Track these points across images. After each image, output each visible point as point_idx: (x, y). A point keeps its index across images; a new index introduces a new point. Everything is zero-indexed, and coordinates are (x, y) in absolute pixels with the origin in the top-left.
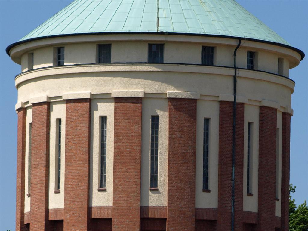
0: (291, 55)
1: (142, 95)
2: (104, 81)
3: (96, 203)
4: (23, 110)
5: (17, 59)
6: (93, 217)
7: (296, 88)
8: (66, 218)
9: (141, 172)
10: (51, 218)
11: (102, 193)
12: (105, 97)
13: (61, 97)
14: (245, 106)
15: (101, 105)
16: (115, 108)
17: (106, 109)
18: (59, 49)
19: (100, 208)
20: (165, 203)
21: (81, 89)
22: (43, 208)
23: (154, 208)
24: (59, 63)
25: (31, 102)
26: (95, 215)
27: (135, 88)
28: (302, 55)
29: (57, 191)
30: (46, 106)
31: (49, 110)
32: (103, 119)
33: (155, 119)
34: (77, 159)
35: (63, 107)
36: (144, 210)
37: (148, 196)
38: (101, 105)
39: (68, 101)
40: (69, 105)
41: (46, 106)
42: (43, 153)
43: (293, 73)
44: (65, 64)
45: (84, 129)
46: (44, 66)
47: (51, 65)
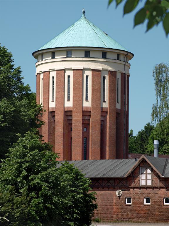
0: (128, 55)
1: (101, 69)
2: (88, 63)
3: (66, 105)
4: (39, 74)
5: (36, 57)
6: (84, 110)
7: (131, 67)
8: (74, 110)
9: (100, 95)
10: (50, 110)
11: (87, 102)
12: (70, 69)
13: (71, 68)
14: (117, 73)
15: (86, 72)
16: (92, 73)
17: (89, 73)
18: (53, 53)
19: (87, 107)
20: (90, 106)
21: (80, 66)
22: (48, 107)
23: (104, 108)
24: (53, 57)
25: (43, 71)
26: (85, 109)
27: (99, 67)
28: (133, 55)
29: (53, 101)
30: (64, 71)
31: (65, 72)
32: (69, 77)
33: (104, 77)
34: (78, 90)
35: (55, 72)
36: (102, 108)
37: (103, 103)
38: (86, 72)
39: (74, 70)
40: (74, 71)
41: (64, 71)
42: (62, 87)
43: (130, 62)
44: (56, 57)
45: (81, 79)
46: (48, 59)
47: (66, 57)
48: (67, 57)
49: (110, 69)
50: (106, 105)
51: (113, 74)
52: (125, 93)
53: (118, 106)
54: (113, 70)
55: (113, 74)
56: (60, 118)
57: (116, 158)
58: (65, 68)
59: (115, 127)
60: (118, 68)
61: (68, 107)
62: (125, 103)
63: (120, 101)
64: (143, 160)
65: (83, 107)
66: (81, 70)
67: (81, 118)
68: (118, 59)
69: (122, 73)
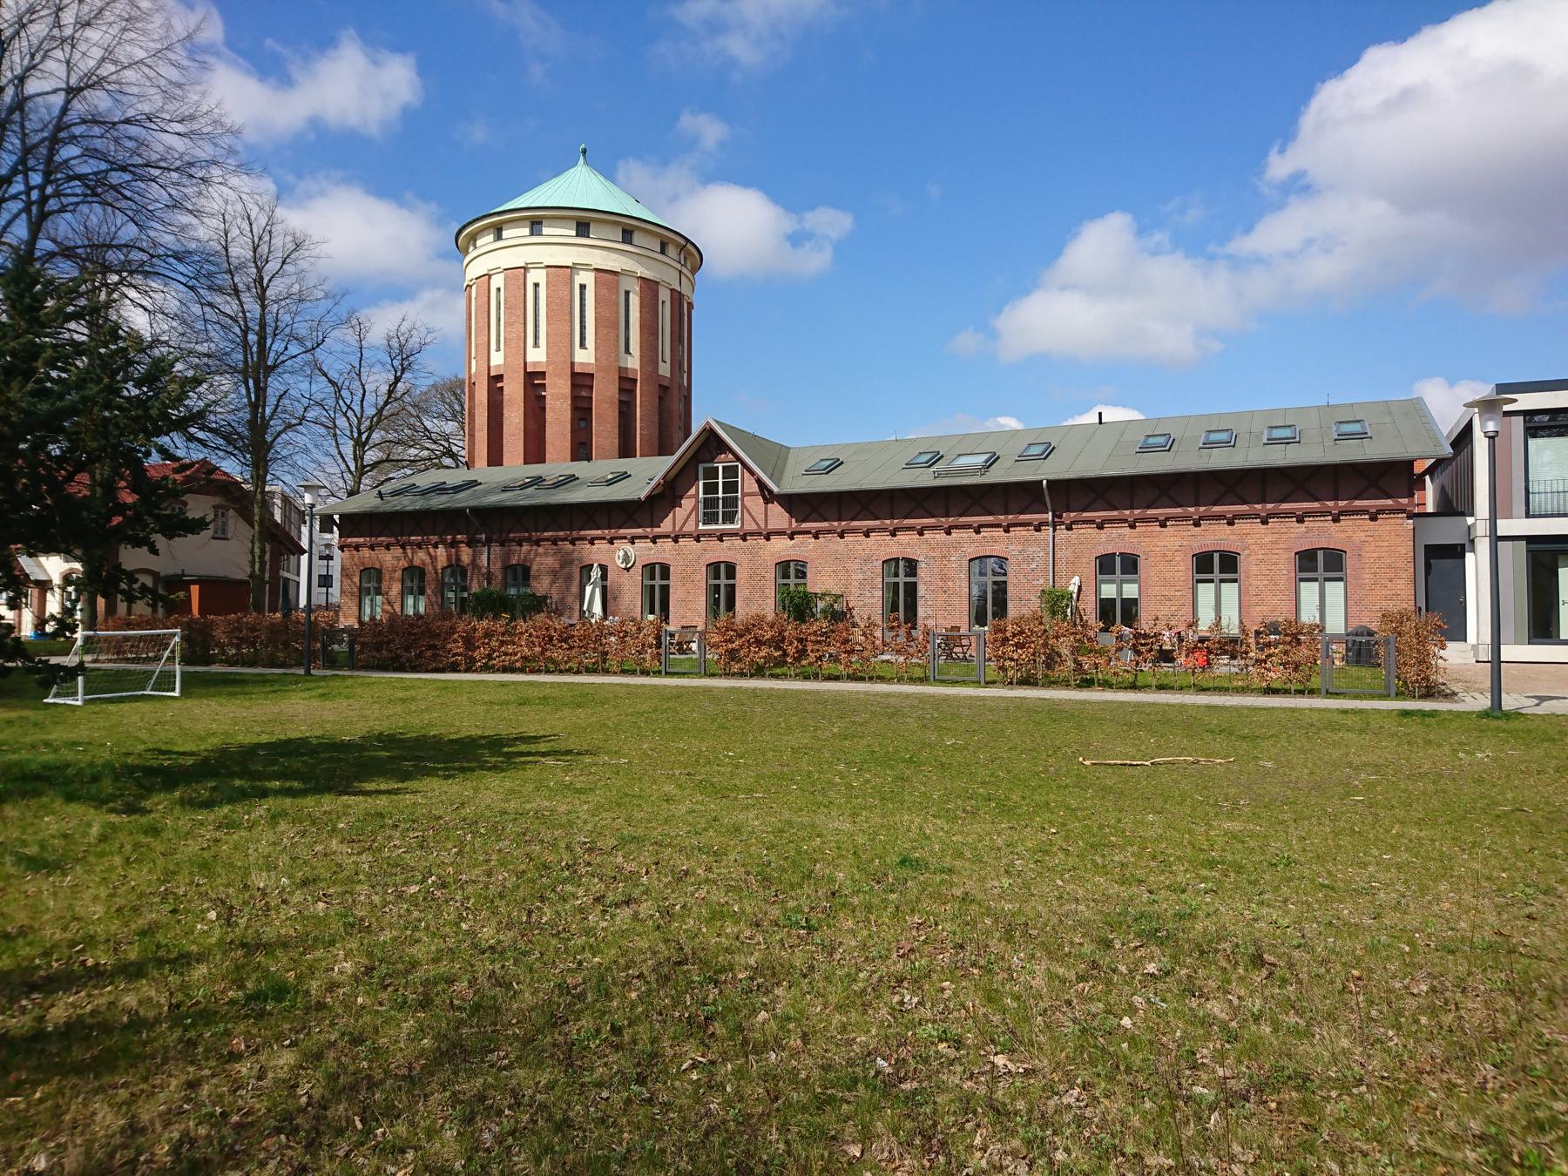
8: (549, 370)
17: (587, 278)
26: (577, 370)
29: (498, 349)
48: (532, 234)
49: (641, 271)
50: (633, 362)
51: (650, 287)
52: (681, 341)
53: (665, 370)
54: (648, 274)
55: (650, 287)
56: (514, 391)
57: (660, 455)
58: (1502, 388)
59: (656, 419)
60: (665, 273)
61: (535, 364)
62: (682, 364)
63: (668, 359)
64: (707, 441)
65: (572, 364)
66: (615, 273)
67: (567, 390)
68: (663, 252)
69: (672, 290)
